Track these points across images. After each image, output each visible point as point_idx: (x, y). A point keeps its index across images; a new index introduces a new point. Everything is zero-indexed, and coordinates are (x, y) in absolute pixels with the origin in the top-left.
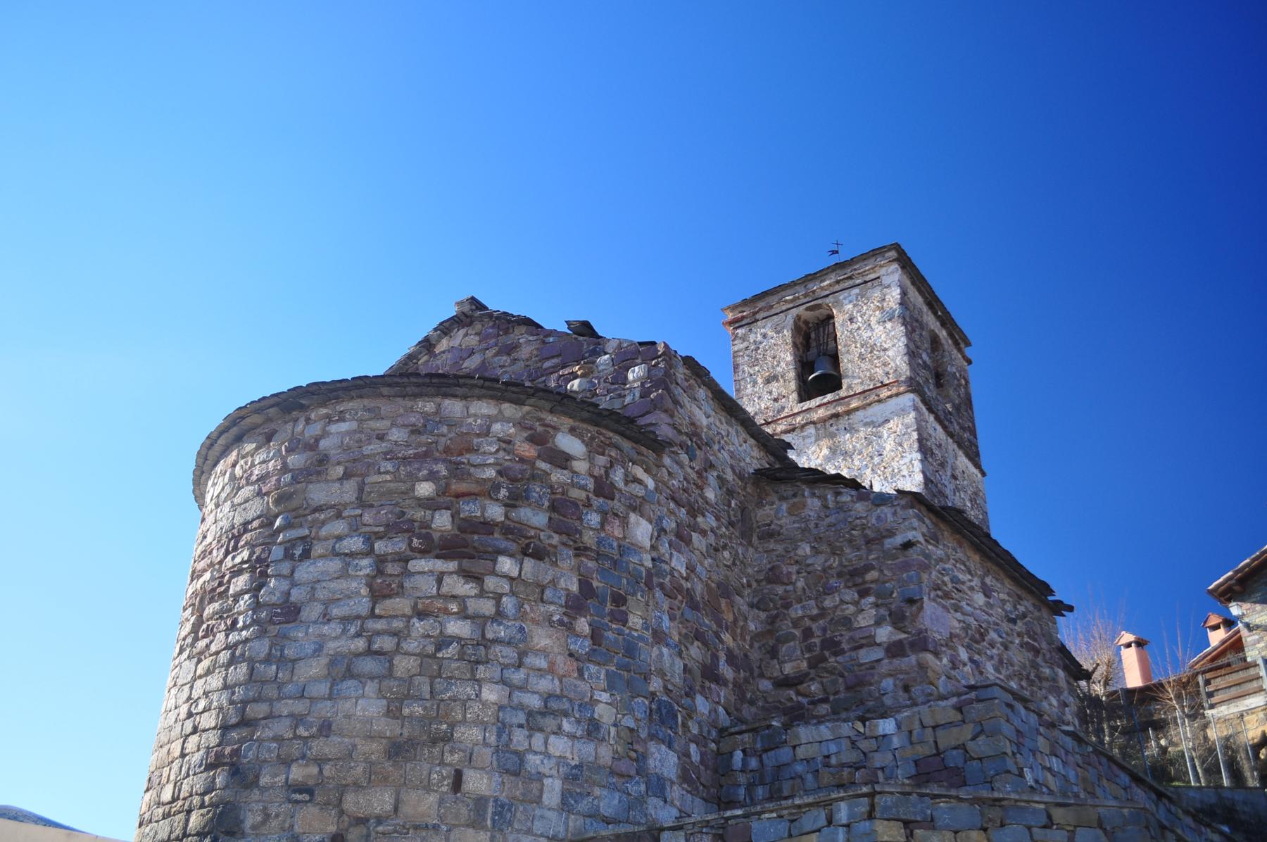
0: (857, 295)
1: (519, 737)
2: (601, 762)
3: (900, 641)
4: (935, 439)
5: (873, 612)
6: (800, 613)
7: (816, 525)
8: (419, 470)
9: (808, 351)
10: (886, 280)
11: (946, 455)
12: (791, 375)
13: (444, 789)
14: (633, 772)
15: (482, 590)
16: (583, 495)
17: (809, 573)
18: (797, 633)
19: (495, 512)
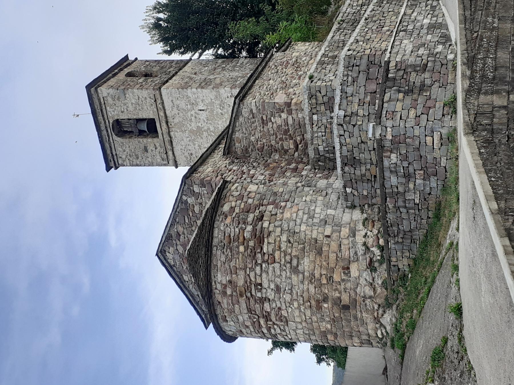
0: (110, 108)
1: (315, 220)
2: (323, 199)
3: (287, 110)
4: (179, 80)
5: (276, 118)
7: (245, 134)
8: (236, 251)
9: (133, 132)
10: (105, 95)
11: (186, 76)
12: (145, 140)
13: (330, 240)
14: (326, 192)
15: (273, 231)
16: (243, 204)
17: (261, 138)
18: (280, 143)
19: (249, 228)
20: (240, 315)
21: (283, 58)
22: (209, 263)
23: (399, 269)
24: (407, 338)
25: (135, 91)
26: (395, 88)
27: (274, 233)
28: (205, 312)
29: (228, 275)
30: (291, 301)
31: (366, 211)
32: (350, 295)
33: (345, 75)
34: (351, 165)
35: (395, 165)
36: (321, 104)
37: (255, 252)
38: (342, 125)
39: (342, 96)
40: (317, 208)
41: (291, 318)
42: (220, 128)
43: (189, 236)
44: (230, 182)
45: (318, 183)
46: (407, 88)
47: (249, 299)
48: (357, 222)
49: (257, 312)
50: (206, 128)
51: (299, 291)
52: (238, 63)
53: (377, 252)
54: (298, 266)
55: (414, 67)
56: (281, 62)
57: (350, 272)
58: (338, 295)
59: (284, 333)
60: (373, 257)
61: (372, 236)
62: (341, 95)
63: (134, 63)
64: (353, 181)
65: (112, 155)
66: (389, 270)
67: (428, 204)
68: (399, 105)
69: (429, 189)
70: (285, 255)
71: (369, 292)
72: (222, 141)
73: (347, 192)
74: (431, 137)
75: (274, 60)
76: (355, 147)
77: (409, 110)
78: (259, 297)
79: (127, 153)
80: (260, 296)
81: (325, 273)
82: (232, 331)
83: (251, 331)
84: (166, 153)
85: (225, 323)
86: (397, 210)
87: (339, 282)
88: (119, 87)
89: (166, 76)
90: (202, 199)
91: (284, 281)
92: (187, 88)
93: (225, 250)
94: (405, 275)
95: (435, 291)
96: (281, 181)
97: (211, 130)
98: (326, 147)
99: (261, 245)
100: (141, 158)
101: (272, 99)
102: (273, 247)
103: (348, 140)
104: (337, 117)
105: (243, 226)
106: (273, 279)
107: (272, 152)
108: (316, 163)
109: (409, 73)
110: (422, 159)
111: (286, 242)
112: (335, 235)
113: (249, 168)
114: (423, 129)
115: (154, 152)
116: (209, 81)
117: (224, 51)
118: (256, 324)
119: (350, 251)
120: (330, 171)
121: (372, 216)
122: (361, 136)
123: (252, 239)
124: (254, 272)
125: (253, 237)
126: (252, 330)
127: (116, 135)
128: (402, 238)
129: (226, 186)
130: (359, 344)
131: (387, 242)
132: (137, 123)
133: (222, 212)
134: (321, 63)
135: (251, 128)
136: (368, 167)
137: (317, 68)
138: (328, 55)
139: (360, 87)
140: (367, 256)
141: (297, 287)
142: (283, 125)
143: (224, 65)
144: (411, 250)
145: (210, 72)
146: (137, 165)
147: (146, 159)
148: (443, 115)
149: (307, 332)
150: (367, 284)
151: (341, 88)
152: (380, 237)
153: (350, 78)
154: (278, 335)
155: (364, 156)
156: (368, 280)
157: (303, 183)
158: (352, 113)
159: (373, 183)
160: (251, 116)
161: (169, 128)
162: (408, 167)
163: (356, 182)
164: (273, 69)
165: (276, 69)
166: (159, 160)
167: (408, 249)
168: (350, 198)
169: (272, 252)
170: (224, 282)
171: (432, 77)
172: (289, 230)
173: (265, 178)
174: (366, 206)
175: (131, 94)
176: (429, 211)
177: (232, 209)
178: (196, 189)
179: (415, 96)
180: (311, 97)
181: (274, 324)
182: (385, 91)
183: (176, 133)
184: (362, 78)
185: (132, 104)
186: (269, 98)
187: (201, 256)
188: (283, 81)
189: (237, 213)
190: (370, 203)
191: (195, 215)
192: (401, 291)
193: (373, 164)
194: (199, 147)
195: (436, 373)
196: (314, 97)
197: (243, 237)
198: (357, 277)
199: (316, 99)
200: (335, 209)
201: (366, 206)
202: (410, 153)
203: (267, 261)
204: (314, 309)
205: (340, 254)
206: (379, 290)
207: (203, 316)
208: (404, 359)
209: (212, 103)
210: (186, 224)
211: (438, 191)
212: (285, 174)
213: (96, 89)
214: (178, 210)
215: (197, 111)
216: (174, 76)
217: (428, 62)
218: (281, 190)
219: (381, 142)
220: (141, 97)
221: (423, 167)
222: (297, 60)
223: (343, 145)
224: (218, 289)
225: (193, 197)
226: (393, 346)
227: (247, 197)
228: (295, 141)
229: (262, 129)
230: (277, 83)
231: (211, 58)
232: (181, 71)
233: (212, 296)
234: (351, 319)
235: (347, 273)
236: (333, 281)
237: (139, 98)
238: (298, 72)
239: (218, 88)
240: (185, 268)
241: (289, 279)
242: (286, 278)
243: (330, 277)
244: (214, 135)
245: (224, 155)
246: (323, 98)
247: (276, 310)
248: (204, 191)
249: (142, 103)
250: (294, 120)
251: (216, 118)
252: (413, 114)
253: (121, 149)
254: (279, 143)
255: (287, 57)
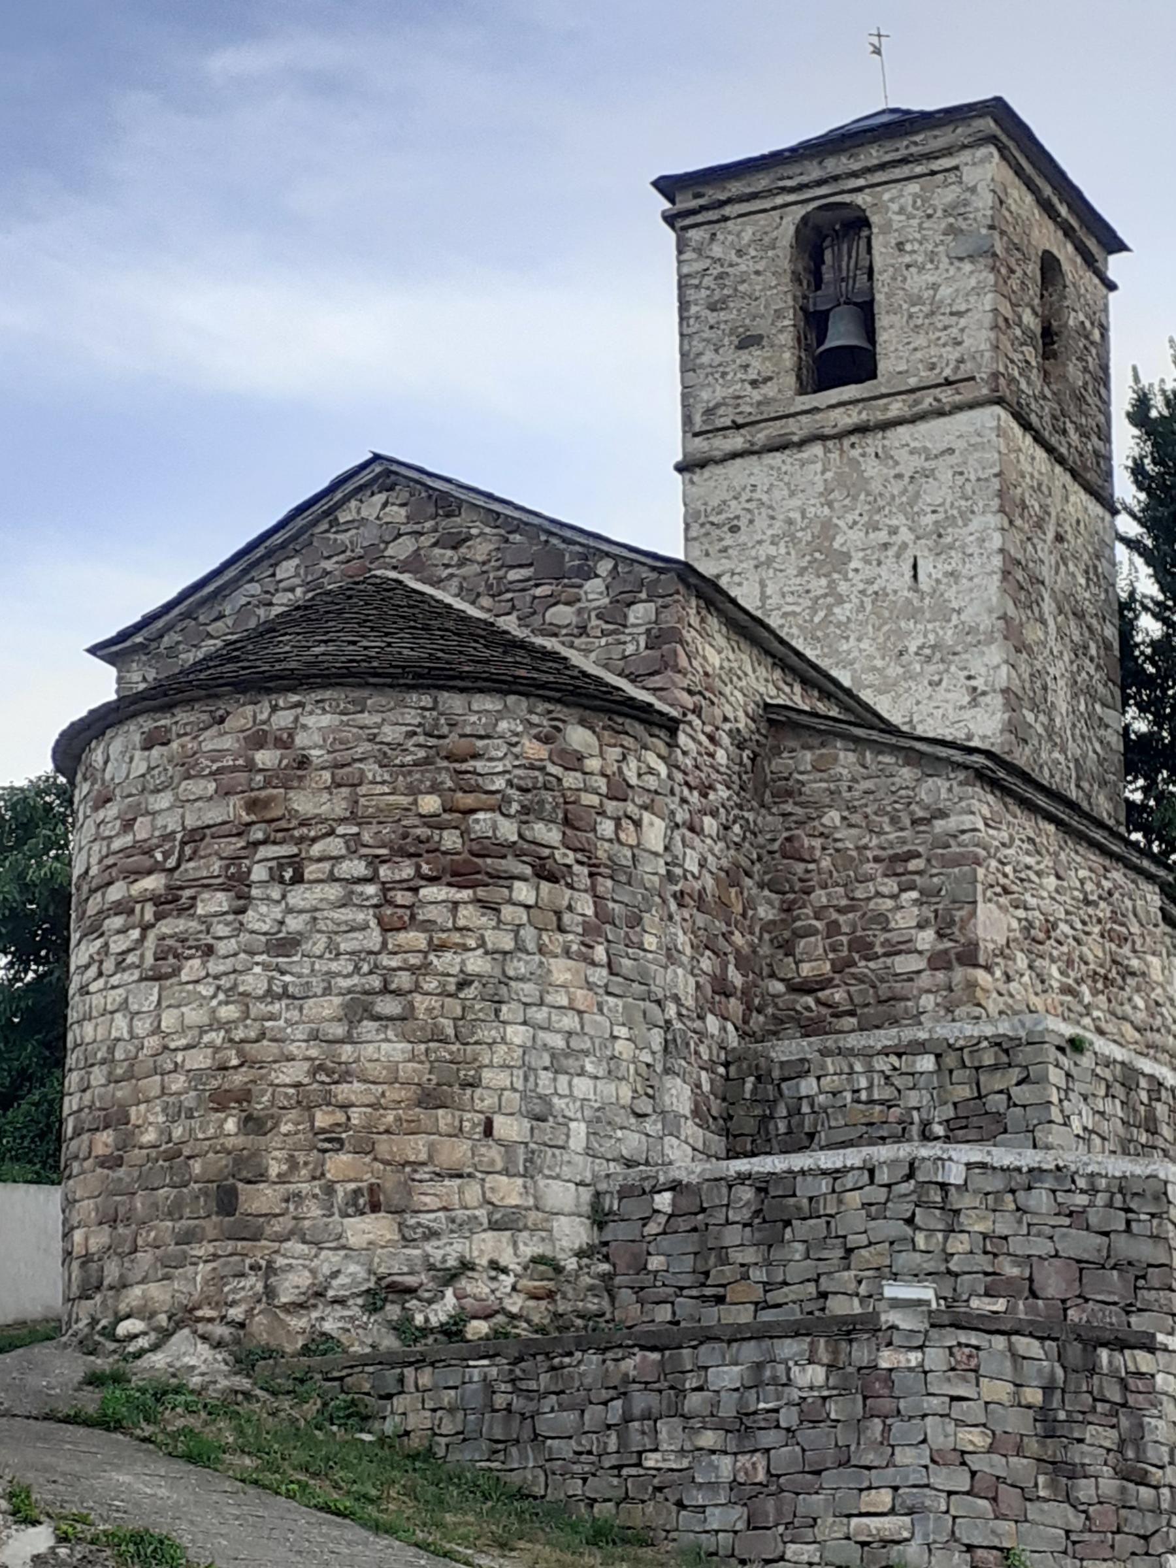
0: (915, 196)
1: (545, 1077)
2: (622, 1102)
3: (946, 952)
4: (1032, 477)
5: (915, 910)
6: (824, 900)
7: (850, 789)
8: (421, 782)
10: (970, 175)
12: (786, 338)
13: (476, 1137)
14: (649, 1110)
15: (499, 921)
17: (837, 850)
18: (818, 924)
19: (508, 830)
20: (177, 799)
21: (1140, 922)
22: (372, 680)
23: (389, 1397)
24: (147, 1434)
25: (988, 300)
26: (1060, 1372)
27: (493, 923)
28: (154, 645)
29: (329, 752)
30: (240, 994)
31: (588, 1266)
32: (276, 1216)
33: (1092, 1184)
34: (761, 1210)
35: (784, 1380)
36: (978, 1084)
37: (420, 855)
38: (910, 1176)
39: (1015, 1174)
40: (590, 1082)
41: (175, 993)
42: (845, 647)
43: (455, 582)
44: (672, 745)
45: (679, 1081)
46: (1062, 1415)
47: (239, 835)
48: (544, 1234)
49: (191, 864)
50: (843, 587)
51: (282, 1023)
52: (1104, 705)
53: (441, 1312)
54: (377, 1018)
55: (1136, 1438)
56: (1123, 915)
57: (362, 1213)
58: (274, 1170)
59: (109, 965)
60: (420, 1300)
61: (498, 1294)
62: (1019, 1170)
63: (1096, 281)
64: (700, 1217)
65: (722, 204)
66: (378, 1359)
67: (643, 1502)
68: (1000, 1391)
69: (700, 1502)
70: (412, 969)
71: (291, 1286)
72: (816, 694)
73: (657, 1197)
74: (889, 1506)
75: (1132, 886)
76: (828, 1223)
77: (984, 1425)
78: (249, 872)
79: (731, 265)
80: (254, 877)
81: (354, 1121)
82: (106, 763)
83: (110, 837)
84: (737, 427)
85: (137, 738)
86: (615, 1388)
87: (323, 1174)
88: (1003, 233)
89: (1047, 419)
90: (604, 633)
91: (317, 967)
92: (1001, 510)
93: (421, 739)
94: (365, 1418)
95: (349, 1536)
96: (682, 940)
97: (836, 610)
98: (812, 1106)
99: (448, 878)
100: (712, 321)
101: (989, 893)
102: (439, 921)
103: (854, 1199)
104: (940, 1159)
105: (515, 807)
106: (321, 925)
107: (784, 893)
108: (750, 1066)
109: (1114, 1420)
110: (809, 1476)
111: (462, 971)
112: (494, 1154)
113: (722, 810)
114: (919, 1477)
115: (739, 375)
116: (1034, 596)
117: (1153, 644)
118: (138, 860)
119: (441, 1214)
120: (721, 1122)
121: (567, 1288)
122: (871, 1249)
123: (468, 843)
124: (344, 852)
125: (475, 847)
126: (117, 845)
127: (805, 219)
128: (508, 1409)
129: (656, 731)
130: (78, 1250)
131: (488, 1349)
132: (856, 304)
133: (564, 721)
134: (1129, 1077)
135: (876, 814)
136: (758, 1274)
137: (1108, 1063)
138: (1159, 1100)
139: (1051, 1238)
140: (423, 1278)
141: (294, 1015)
142: (888, 935)
143: (1093, 651)
144: (464, 1440)
145: (1067, 597)
146: (683, 305)
147: (708, 341)
148: (970, 1548)
149: (119, 1054)
150: (322, 1279)
151: (1045, 1166)
152: (494, 1320)
153: (1082, 1200)
154: (99, 943)
155: (797, 1257)
156: (335, 1283)
157: (677, 1025)
158: (957, 1212)
159: (694, 1292)
160: (920, 814)
161: (840, 436)
162: (778, 1426)
163: (695, 1230)
164: (1099, 885)
165: (1100, 897)
166: (705, 395)
167: (468, 1429)
168: (634, 1208)
169: (420, 917)
170: (301, 739)
171: (1100, 1503)
172: (506, 980)
173: (689, 877)
174: (605, 1267)
175: (973, 282)
176: (618, 1504)
177: (574, 762)
178: (640, 613)
179: (1033, 1446)
180: (1005, 1046)
181: (146, 928)
182: (1049, 1338)
183: (819, 467)
184: (1085, 1244)
185: (935, 287)
186: (991, 879)
187: (389, 645)
188: (1054, 926)
189: (559, 780)
190: (618, 1280)
191: (540, 609)
192: (306, 1406)
193: (766, 1291)
194: (763, 559)
195: (94, 1547)
196: (1005, 1059)
197: (474, 806)
198: (343, 1241)
199: (995, 1067)
200: (589, 1152)
201: (605, 1267)
202: (828, 1434)
203: (390, 903)
204: (215, 1084)
205: (427, 1176)
206: (297, 1323)
207: (138, 639)
208: (70, 1427)
209: (944, 613)
210: (501, 573)
211: (692, 1535)
212: (708, 953)
213: (993, 140)
214: (554, 541)
215: (908, 555)
216: (1050, 450)
217: (1156, 1487)
218: (650, 942)
219: (867, 1331)
220: (963, 322)
221: (782, 1480)
222: (1133, 974)
223: (835, 1179)
224: (273, 718)
225: (607, 600)
226: (94, 1380)
227: (621, 813)
228: (825, 983)
229: (869, 854)
230: (1046, 905)
231: (1122, 592)
232: (1068, 478)
233: (244, 692)
234: (183, 1221)
235: (355, 1204)
236: (325, 1151)
237: (959, 314)
238: (1089, 981)
239: (1006, 638)
240: (328, 565)
241: (323, 985)
242: (327, 973)
243: (340, 1141)
244: (817, 620)
245: (767, 705)
246: (1001, 1092)
247: (201, 936)
248: (634, 645)
249: (940, 325)
250: (911, 980)
251: (886, 628)
252: (971, 1442)
253: (747, 236)
254: (817, 919)
255: (1142, 935)
